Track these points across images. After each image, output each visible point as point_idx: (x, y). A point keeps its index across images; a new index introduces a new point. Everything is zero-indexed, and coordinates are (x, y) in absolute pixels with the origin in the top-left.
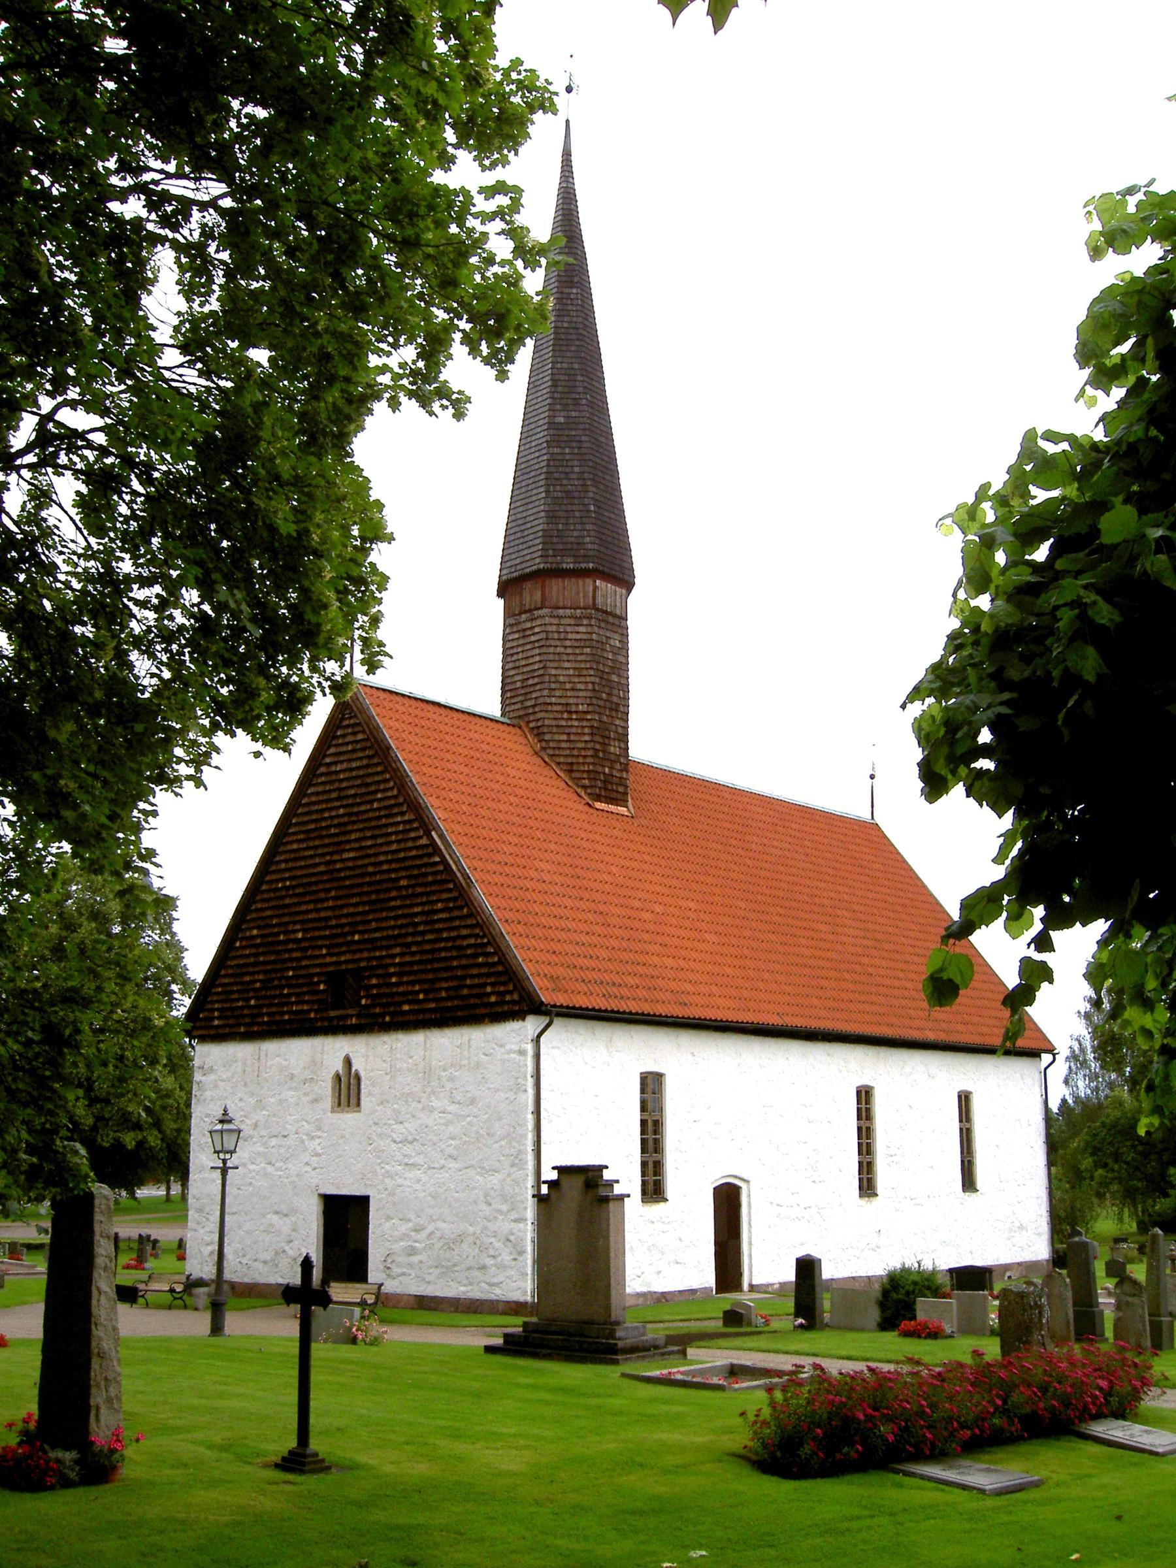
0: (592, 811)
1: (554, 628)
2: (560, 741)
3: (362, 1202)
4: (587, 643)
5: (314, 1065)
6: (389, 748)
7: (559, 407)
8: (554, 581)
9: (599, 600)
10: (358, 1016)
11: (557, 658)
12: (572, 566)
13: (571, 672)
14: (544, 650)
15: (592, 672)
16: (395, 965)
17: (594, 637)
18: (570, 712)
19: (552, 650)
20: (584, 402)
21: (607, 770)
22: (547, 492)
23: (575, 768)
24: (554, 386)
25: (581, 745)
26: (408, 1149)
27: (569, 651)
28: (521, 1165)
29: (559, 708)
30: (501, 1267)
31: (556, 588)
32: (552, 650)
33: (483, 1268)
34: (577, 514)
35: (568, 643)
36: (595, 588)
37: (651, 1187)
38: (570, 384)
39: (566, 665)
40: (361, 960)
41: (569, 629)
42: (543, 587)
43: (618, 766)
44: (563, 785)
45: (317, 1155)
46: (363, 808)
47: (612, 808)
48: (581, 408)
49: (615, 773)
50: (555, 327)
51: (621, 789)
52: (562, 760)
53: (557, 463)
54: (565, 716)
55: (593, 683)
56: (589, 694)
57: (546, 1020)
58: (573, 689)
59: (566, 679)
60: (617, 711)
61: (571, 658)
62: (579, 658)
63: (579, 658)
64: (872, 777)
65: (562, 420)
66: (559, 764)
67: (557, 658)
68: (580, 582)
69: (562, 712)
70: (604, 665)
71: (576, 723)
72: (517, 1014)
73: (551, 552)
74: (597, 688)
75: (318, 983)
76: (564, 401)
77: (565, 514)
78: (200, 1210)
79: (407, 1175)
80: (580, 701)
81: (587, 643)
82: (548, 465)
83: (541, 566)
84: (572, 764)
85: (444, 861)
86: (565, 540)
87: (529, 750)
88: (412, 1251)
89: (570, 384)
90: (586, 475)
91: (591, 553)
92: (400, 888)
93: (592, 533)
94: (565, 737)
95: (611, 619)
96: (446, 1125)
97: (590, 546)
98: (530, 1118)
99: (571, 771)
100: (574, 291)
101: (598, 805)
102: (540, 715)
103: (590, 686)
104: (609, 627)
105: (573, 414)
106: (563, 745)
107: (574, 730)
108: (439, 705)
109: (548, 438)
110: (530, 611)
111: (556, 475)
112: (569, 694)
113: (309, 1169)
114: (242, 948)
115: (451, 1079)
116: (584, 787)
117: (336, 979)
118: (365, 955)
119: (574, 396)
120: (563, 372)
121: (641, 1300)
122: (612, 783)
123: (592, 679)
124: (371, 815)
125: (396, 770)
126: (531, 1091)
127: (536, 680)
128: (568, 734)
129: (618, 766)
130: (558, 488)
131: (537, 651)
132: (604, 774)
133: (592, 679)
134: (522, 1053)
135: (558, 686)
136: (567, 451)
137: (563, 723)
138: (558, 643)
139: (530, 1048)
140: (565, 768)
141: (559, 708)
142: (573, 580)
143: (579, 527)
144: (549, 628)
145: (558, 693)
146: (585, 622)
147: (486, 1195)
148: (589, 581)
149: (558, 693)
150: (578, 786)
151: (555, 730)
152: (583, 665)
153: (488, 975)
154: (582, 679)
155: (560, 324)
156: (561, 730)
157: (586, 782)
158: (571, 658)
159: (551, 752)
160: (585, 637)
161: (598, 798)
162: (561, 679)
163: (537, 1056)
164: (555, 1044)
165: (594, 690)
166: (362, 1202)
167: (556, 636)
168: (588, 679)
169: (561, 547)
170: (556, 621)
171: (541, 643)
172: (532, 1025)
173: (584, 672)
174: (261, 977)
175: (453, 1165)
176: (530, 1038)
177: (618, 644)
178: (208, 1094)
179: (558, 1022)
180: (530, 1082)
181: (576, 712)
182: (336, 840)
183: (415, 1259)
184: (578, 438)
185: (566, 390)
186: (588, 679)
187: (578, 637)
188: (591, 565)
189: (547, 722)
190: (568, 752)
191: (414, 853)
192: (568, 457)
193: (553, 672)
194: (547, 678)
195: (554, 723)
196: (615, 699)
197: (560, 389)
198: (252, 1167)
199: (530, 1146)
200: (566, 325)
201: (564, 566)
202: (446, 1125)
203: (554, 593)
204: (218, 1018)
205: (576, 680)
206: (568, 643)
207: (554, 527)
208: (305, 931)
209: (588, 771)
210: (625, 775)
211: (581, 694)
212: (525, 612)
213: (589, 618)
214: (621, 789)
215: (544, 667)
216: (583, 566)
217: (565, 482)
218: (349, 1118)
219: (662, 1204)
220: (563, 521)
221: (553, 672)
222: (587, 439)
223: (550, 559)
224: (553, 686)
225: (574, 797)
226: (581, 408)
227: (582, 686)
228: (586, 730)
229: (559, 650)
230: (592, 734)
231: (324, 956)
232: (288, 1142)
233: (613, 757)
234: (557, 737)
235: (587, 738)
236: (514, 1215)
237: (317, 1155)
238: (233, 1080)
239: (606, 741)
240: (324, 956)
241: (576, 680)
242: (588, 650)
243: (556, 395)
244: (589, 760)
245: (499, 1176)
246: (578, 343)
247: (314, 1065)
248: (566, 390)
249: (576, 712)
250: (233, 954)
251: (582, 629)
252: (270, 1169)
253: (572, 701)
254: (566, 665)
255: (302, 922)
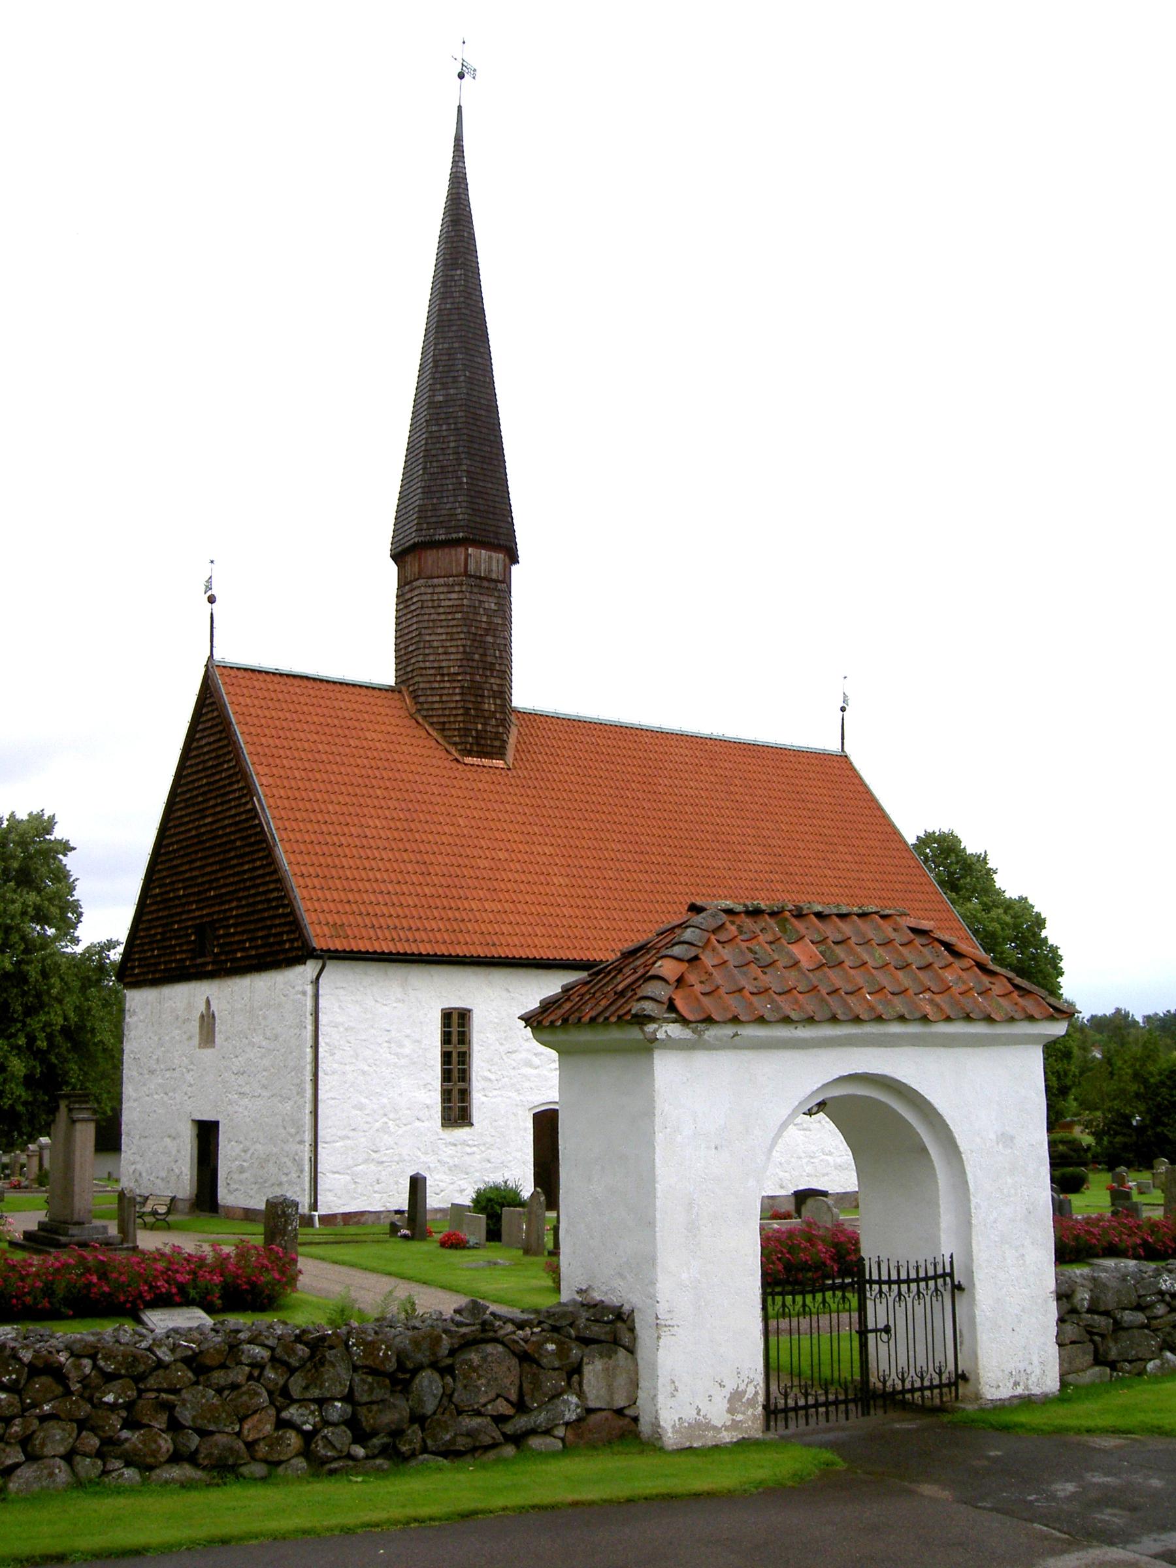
0: (459, 766)
1: (429, 597)
2: (433, 702)
3: (215, 1124)
4: (459, 609)
5: (190, 1006)
6: (231, 723)
7: (438, 386)
8: (429, 552)
9: (472, 568)
10: (213, 963)
11: (431, 624)
12: (443, 537)
13: (444, 637)
14: (420, 618)
15: (462, 636)
16: (232, 917)
17: (465, 602)
18: (443, 675)
19: (426, 617)
20: (462, 379)
21: (480, 727)
22: (424, 468)
23: (447, 726)
24: (436, 366)
25: (453, 705)
26: (241, 1080)
27: (443, 617)
28: (301, 1093)
29: (432, 672)
30: (290, 1183)
31: (430, 556)
32: (426, 617)
33: (280, 1184)
34: (450, 487)
35: (441, 610)
36: (467, 556)
37: (455, 1113)
38: (450, 363)
39: (440, 630)
40: (214, 913)
41: (442, 597)
42: (420, 559)
43: (493, 722)
44: (433, 743)
45: (191, 1085)
46: (217, 777)
47: (486, 762)
48: (459, 385)
49: (489, 728)
50: (439, 310)
51: (497, 743)
52: (435, 720)
53: (434, 440)
54: (438, 678)
55: (463, 646)
56: (459, 656)
57: (320, 963)
58: (445, 653)
59: (439, 644)
60: (492, 670)
61: (444, 623)
62: (451, 623)
63: (451, 623)
64: (843, 709)
65: (441, 398)
66: (432, 724)
67: (431, 624)
68: (453, 552)
69: (435, 675)
70: (477, 627)
71: (448, 685)
72: (300, 960)
73: (425, 526)
74: (468, 650)
75: (190, 935)
76: (444, 380)
77: (439, 488)
78: (128, 1135)
79: (241, 1103)
80: (451, 663)
81: (459, 609)
82: (426, 444)
83: (416, 540)
84: (444, 723)
85: (260, 824)
86: (438, 513)
87: (403, 713)
88: (242, 1170)
89: (450, 363)
90: (461, 449)
91: (462, 523)
92: (236, 848)
93: (464, 504)
94: (437, 698)
95: (485, 584)
96: (261, 1058)
97: (460, 517)
98: (309, 1050)
99: (443, 730)
100: (458, 272)
101: (469, 760)
102: (416, 679)
103: (461, 649)
104: (482, 591)
105: (452, 391)
106: (436, 706)
107: (446, 692)
108: (307, 678)
109: (428, 418)
110: (411, 582)
111: (433, 452)
112: (441, 657)
113: (186, 1098)
114: (151, 904)
115: (265, 1018)
116: (455, 744)
117: (200, 930)
118: (217, 909)
119: (452, 374)
120: (444, 352)
121: (439, 1216)
122: (485, 739)
123: (464, 642)
124: (221, 783)
125: (234, 743)
126: (310, 1028)
127: (414, 647)
128: (441, 695)
129: (493, 722)
130: (435, 464)
131: (415, 620)
132: (477, 730)
133: (464, 642)
134: (304, 993)
135: (431, 651)
136: (444, 427)
137: (436, 685)
138: (432, 611)
139: (309, 989)
140: (438, 727)
141: (432, 672)
142: (446, 550)
143: (452, 499)
144: (424, 597)
145: (431, 658)
146: (457, 589)
147: (283, 1120)
148: (461, 550)
149: (431, 658)
150: (449, 743)
151: (429, 692)
152: (454, 630)
153: (285, 924)
154: (455, 643)
155: (443, 307)
156: (434, 692)
157: (457, 739)
158: (444, 623)
159: (425, 713)
160: (456, 603)
161: (469, 753)
162: (435, 644)
163: (316, 996)
164: (339, 984)
165: (464, 652)
166: (215, 1124)
167: (430, 604)
168: (459, 643)
169: (434, 519)
170: (430, 590)
171: (418, 612)
172: (309, 969)
173: (456, 636)
174: (160, 930)
175: (266, 1094)
176: (309, 979)
177: (493, 606)
178: (133, 1033)
179: (331, 966)
180: (309, 1020)
181: (448, 675)
182: (201, 807)
183: (244, 1176)
184: (454, 415)
185: (446, 369)
186: (459, 643)
187: (450, 603)
188: (461, 535)
189: (421, 686)
190: (440, 712)
191: (244, 817)
192: (445, 433)
193: (428, 638)
194: (422, 645)
195: (428, 686)
196: (489, 659)
197: (440, 369)
198: (156, 1097)
199: (308, 1077)
200: (448, 306)
201: (437, 537)
202: (261, 1058)
203: (430, 562)
204: (139, 966)
205: (448, 644)
206: (441, 610)
207: (429, 502)
208: (184, 888)
209: (459, 729)
210: (501, 730)
211: (452, 657)
212: (408, 584)
213: (461, 584)
214: (497, 743)
215: (420, 634)
216: (454, 536)
217: (441, 458)
218: (208, 1052)
219: (466, 1129)
220: (438, 495)
221: (428, 638)
222: (463, 414)
223: (424, 533)
224: (427, 651)
225: (443, 754)
226: (459, 385)
227: (453, 650)
228: (457, 691)
229: (432, 617)
230: (462, 694)
231: (194, 911)
232: (176, 1074)
233: (487, 714)
234: (430, 699)
235: (458, 698)
236: (298, 1138)
237: (191, 1085)
238: (156, 1019)
239: (479, 699)
240: (194, 911)
241: (448, 644)
242: (459, 616)
243: (438, 375)
244: (460, 718)
245: (291, 1103)
246: (459, 322)
247: (190, 1006)
248: (446, 369)
249: (448, 675)
250: (147, 910)
251: (454, 596)
252: (166, 1098)
253: (444, 664)
254: (440, 630)
255: (183, 880)
